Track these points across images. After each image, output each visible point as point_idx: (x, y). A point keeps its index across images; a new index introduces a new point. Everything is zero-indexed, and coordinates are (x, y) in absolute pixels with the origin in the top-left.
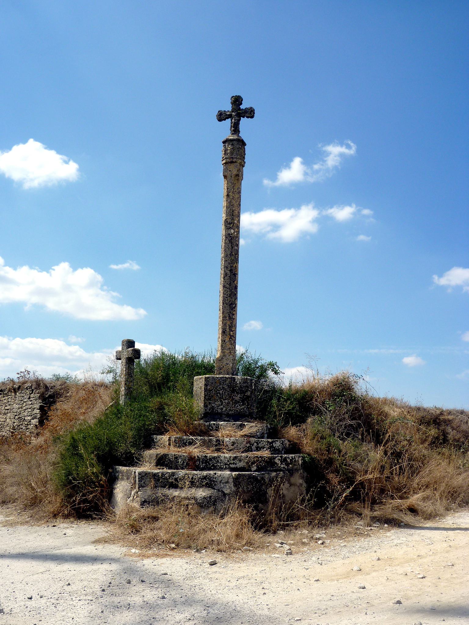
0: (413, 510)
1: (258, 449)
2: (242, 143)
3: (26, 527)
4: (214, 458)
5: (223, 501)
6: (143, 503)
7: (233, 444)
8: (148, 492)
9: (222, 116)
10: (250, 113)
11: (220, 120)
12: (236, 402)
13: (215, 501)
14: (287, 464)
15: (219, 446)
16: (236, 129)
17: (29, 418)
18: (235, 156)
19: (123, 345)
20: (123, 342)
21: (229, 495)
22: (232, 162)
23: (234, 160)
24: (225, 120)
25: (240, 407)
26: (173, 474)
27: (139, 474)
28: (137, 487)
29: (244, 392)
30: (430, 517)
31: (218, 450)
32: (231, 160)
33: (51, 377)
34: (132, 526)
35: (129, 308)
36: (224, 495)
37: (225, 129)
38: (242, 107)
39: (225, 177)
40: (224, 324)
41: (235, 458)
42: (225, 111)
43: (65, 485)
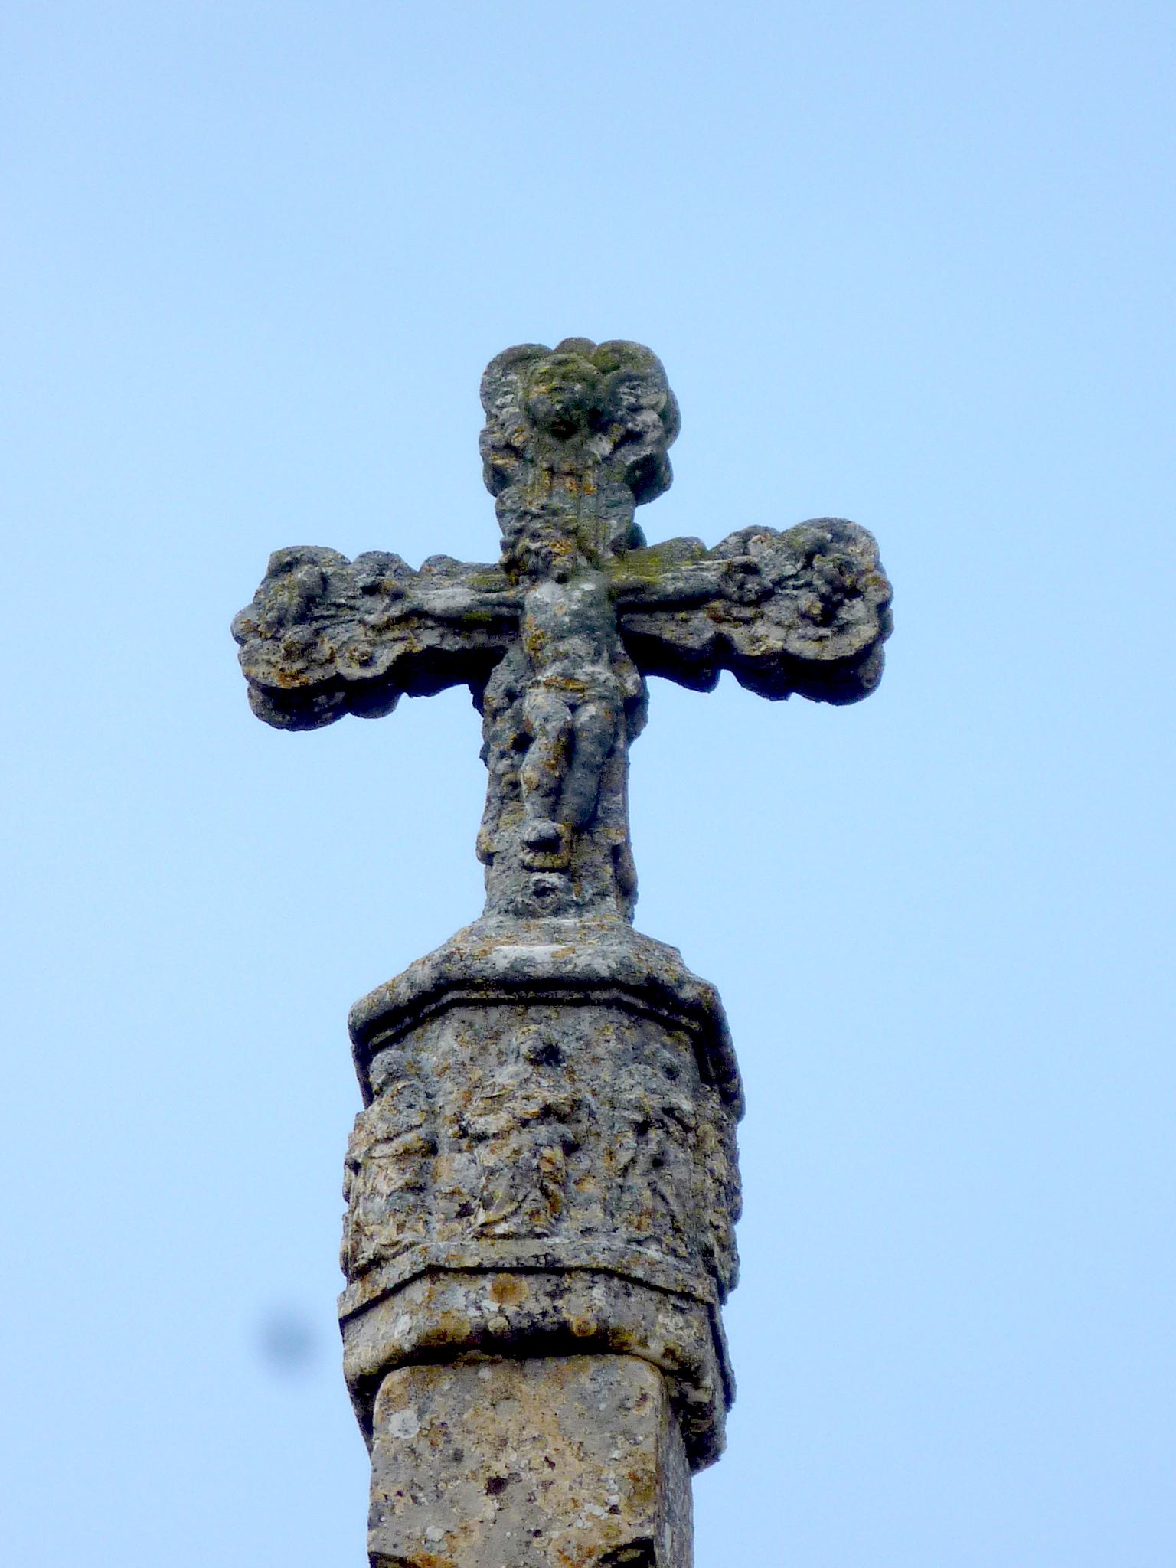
9: (326, 654)
10: (805, 628)
16: (568, 823)
18: (601, 1250)
23: (585, 1306)
24: (371, 698)
32: (530, 1300)
33: (352, 556)
35: (667, 636)
42: (385, 563)
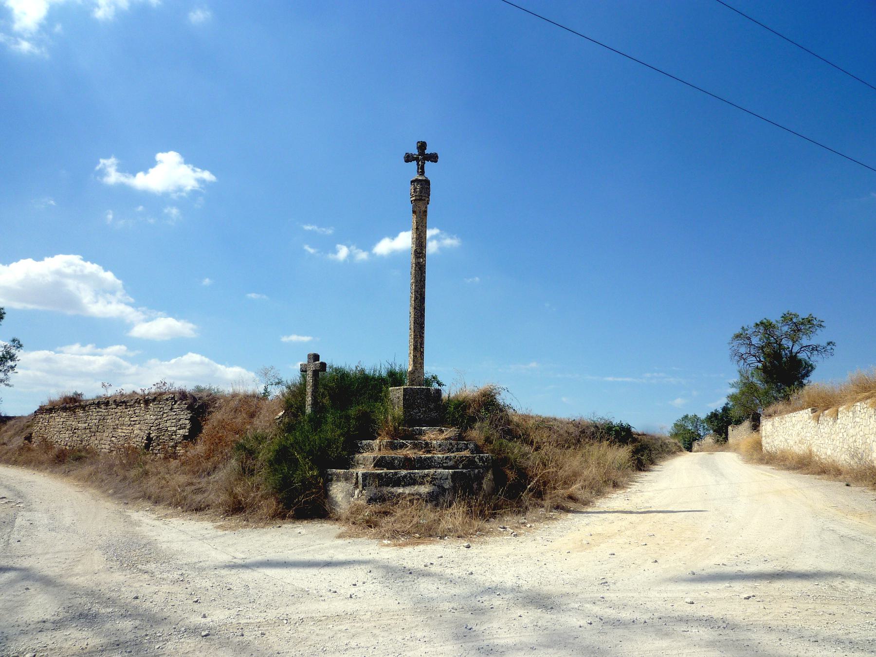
0: (572, 498)
1: (458, 450)
2: (427, 182)
3: (768, 467)
4: (429, 458)
5: (444, 495)
6: (370, 501)
7: (440, 446)
8: (372, 490)
9: (408, 158)
11: (407, 161)
12: (431, 410)
13: (437, 495)
14: (484, 462)
15: (428, 448)
17: (174, 429)
19: (309, 358)
20: (309, 355)
21: (448, 489)
22: (420, 200)
25: (434, 414)
26: (396, 473)
27: (363, 474)
28: (360, 487)
29: (426, 404)
30: (586, 503)
31: (429, 452)
34: (367, 522)
36: (444, 490)
37: (411, 170)
38: (426, 152)
39: (414, 212)
40: (416, 342)
41: (447, 457)
43: (280, 491)
